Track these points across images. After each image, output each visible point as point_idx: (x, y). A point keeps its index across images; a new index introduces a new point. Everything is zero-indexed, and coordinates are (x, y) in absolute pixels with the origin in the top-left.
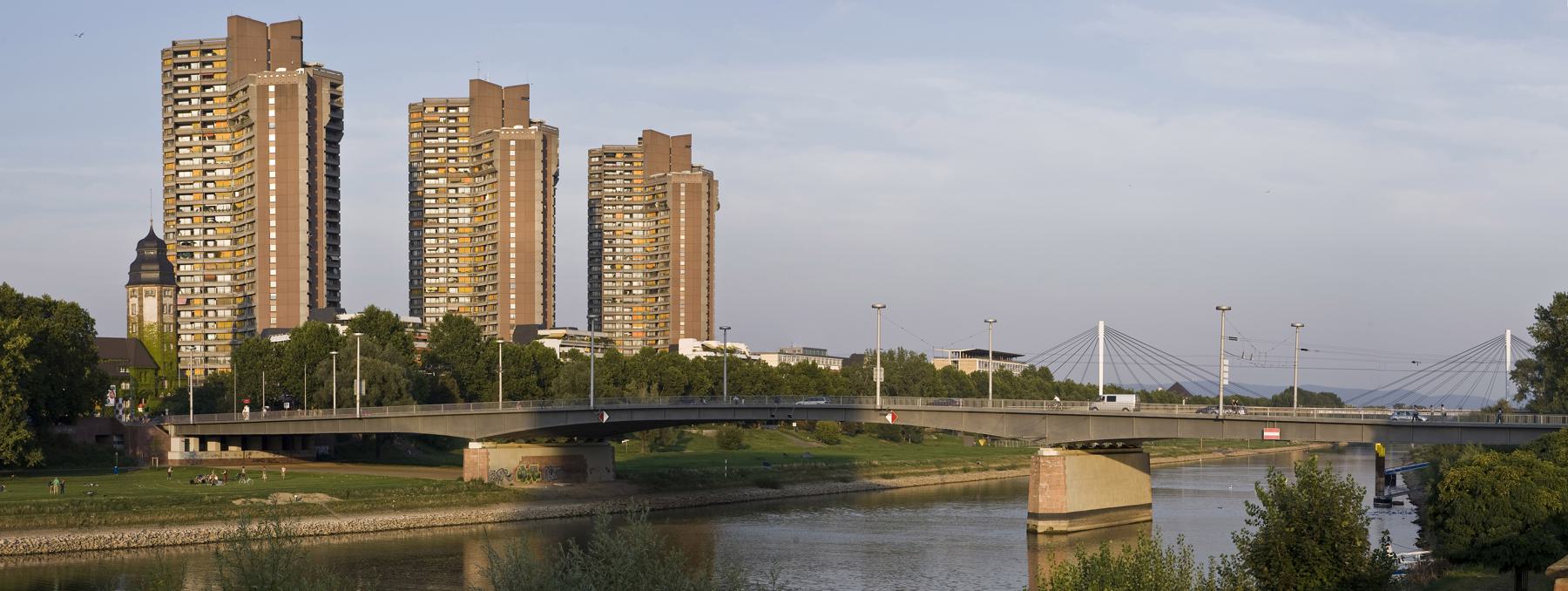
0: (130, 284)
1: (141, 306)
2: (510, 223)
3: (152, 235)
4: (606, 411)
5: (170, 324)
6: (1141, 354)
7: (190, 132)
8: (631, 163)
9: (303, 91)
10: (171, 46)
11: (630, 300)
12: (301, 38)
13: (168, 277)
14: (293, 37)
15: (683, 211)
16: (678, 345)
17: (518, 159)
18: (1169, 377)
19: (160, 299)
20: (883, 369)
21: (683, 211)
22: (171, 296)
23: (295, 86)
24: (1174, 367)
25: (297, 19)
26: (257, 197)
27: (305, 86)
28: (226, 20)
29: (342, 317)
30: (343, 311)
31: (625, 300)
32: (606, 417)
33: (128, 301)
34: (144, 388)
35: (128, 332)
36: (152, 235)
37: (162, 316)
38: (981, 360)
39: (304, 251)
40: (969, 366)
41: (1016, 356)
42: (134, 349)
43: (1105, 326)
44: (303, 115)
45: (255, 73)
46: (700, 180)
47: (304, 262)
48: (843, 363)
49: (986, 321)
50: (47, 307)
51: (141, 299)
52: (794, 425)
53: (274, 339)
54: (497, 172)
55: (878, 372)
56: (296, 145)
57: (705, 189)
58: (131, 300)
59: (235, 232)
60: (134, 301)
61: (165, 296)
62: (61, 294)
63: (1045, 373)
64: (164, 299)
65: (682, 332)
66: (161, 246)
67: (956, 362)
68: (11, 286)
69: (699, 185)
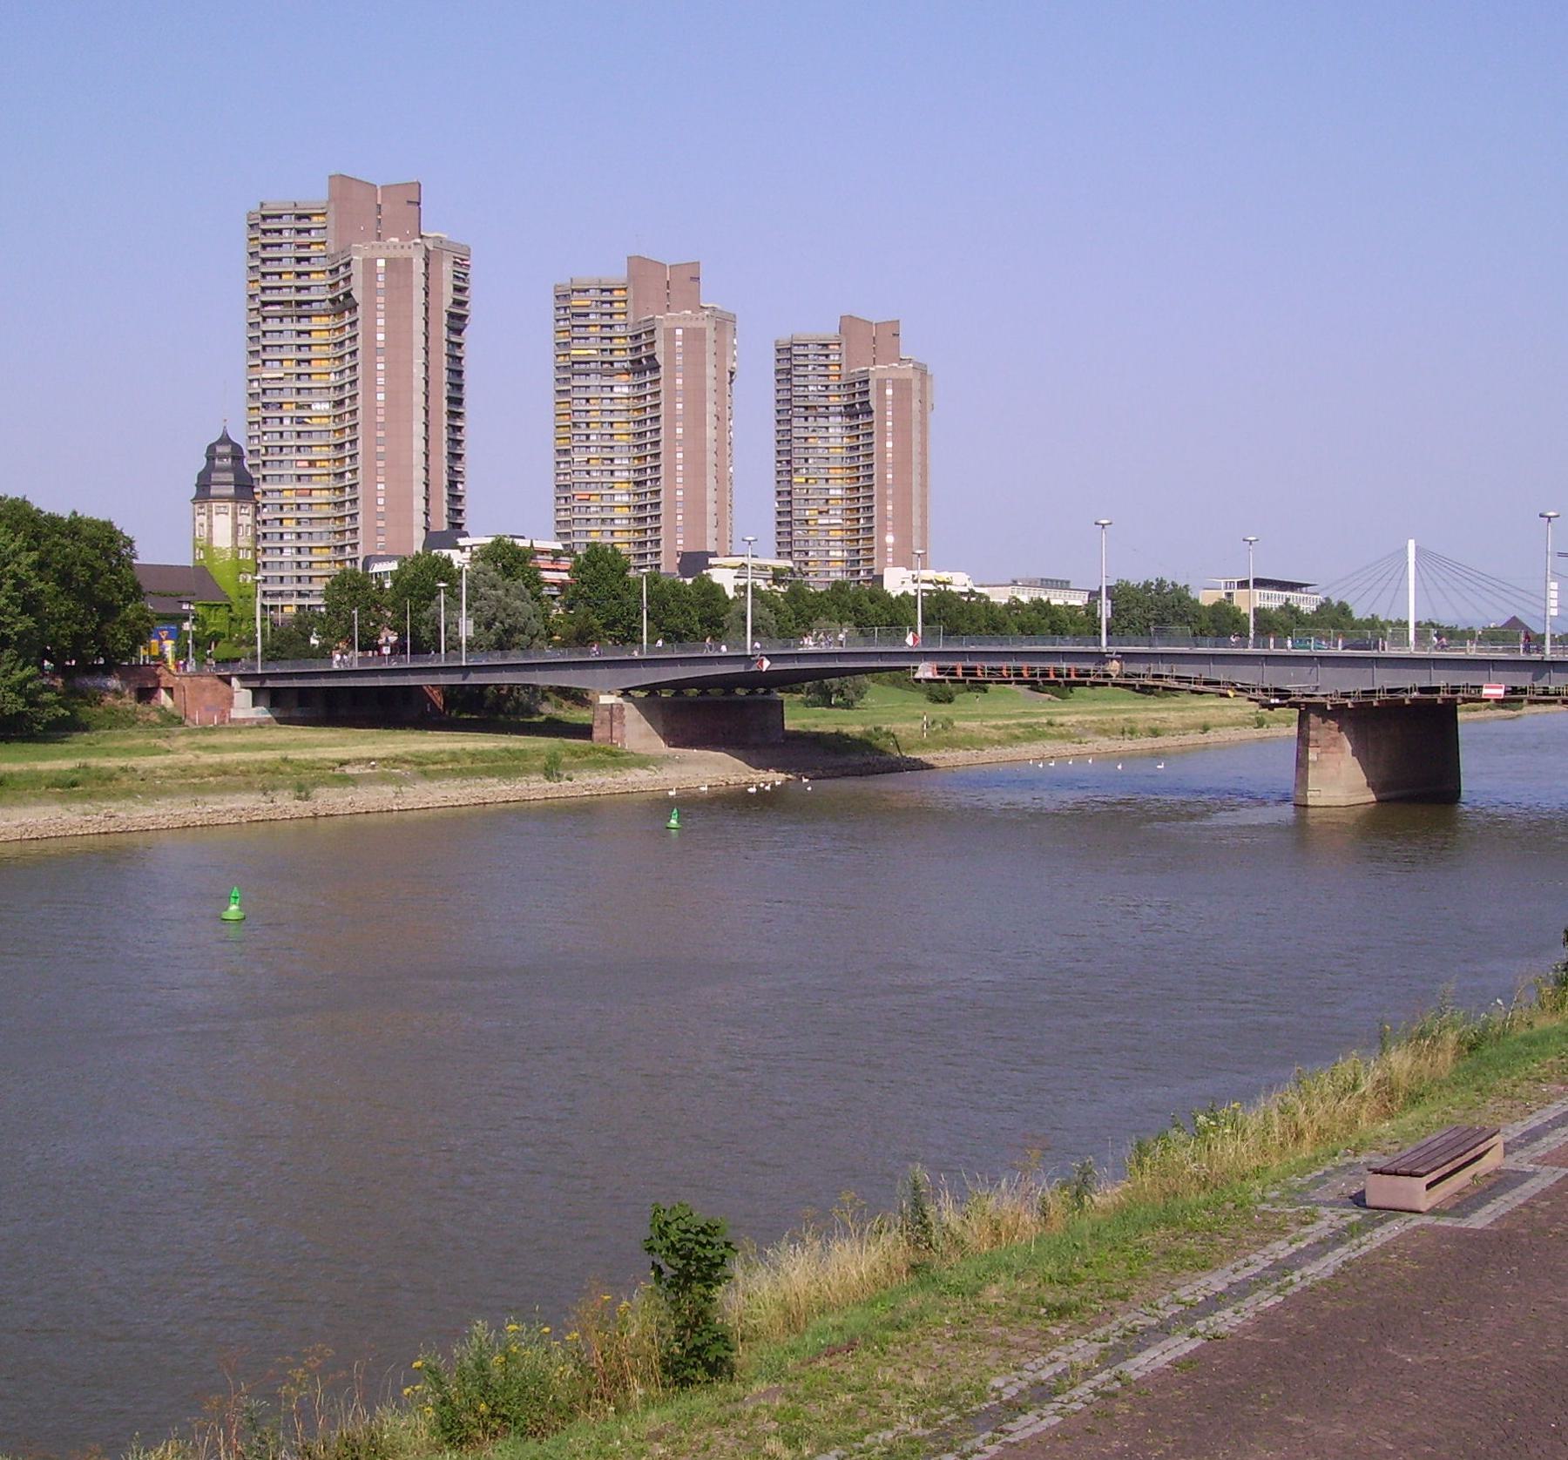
0: (195, 500)
1: (210, 526)
2: (676, 427)
3: (225, 440)
4: (766, 656)
5: (248, 549)
6: (1490, 587)
7: (280, 314)
8: (827, 356)
9: (418, 266)
10: (259, 207)
11: (826, 521)
12: (419, 204)
13: (245, 489)
14: (409, 202)
15: (889, 413)
16: (882, 576)
17: (685, 353)
18: (1502, 611)
19: (235, 516)
20: (1109, 602)
21: (889, 413)
22: (248, 515)
23: (409, 261)
24: (1503, 594)
25: (415, 181)
26: (361, 394)
27: (421, 260)
28: (327, 178)
29: (462, 542)
30: (466, 535)
31: (820, 522)
32: (766, 663)
33: (195, 519)
34: (213, 629)
35: (195, 559)
36: (225, 440)
37: (236, 539)
38: (1262, 591)
39: (418, 460)
40: (1249, 602)
41: (1307, 585)
42: (197, 582)
43: (1417, 548)
44: (419, 296)
45: (360, 243)
46: (910, 375)
47: (419, 474)
48: (1089, 596)
49: (1244, 540)
50: (74, 528)
51: (210, 518)
52: (48, 648)
53: (377, 568)
54: (659, 366)
55: (1104, 606)
56: (410, 330)
57: (916, 385)
58: (197, 518)
59: (603, 464)
60: (203, 519)
61: (241, 514)
62: (93, 509)
63: (1344, 610)
64: (239, 517)
65: (890, 560)
66: (237, 455)
67: (1229, 595)
68: (1136, 579)
69: (909, 381)
